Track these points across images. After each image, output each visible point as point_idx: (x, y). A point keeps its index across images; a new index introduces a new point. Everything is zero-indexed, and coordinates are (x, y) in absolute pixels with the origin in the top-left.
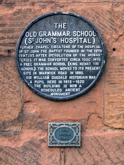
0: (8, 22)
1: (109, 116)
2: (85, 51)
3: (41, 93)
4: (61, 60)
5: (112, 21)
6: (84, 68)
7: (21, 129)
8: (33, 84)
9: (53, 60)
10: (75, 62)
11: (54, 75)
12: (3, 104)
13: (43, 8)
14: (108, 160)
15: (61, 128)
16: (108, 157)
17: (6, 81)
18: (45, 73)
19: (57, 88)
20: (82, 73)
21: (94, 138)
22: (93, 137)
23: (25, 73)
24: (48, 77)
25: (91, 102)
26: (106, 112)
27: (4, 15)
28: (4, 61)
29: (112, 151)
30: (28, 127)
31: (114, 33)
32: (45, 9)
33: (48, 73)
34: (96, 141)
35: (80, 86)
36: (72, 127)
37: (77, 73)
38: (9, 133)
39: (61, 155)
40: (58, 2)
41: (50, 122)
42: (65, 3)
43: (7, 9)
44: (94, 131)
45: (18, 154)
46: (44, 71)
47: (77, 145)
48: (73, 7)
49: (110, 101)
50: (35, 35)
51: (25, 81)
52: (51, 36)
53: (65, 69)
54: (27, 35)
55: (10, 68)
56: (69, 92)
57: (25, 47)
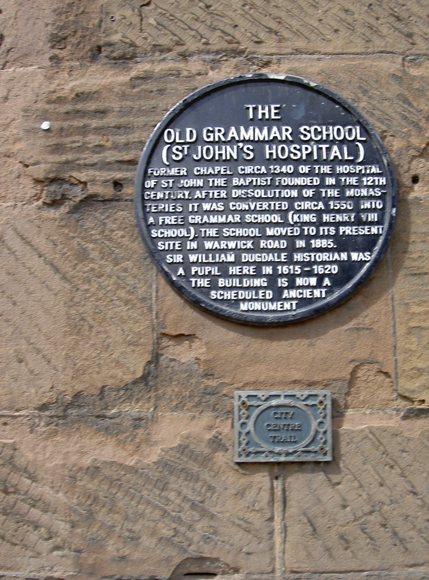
0: (116, 106)
1: (412, 369)
2: (338, 181)
3: (212, 303)
4: (269, 206)
5: (406, 101)
6: (337, 230)
7: (152, 409)
8: (187, 276)
10: (308, 211)
11: (247, 250)
12: (99, 336)
13: (212, 69)
14: (410, 498)
15: (271, 407)
16: (410, 489)
17: (108, 270)
18: (223, 246)
19: (257, 288)
20: (330, 245)
21: (371, 436)
22: (367, 431)
23: (164, 244)
24: (231, 255)
25: (357, 329)
26: (403, 356)
27: (105, 87)
28: (102, 214)
29: (422, 472)
30: (174, 403)
31: (413, 133)
32: (217, 70)
33: (232, 245)
34: (377, 443)
35: (327, 282)
36: (305, 403)
37: (282, 269)
38: (117, 420)
39: (272, 488)
40: (254, 53)
41: (238, 389)
42: (272, 55)
43: (113, 72)
44: (368, 412)
45: (145, 484)
46: (219, 238)
47: (321, 458)
48: (296, 65)
49: (412, 324)
50: (191, 137)
51: (163, 269)
52: (237, 139)
53: (281, 233)
54: (169, 138)
55: (121, 233)
56: (292, 299)
57: (162, 171)
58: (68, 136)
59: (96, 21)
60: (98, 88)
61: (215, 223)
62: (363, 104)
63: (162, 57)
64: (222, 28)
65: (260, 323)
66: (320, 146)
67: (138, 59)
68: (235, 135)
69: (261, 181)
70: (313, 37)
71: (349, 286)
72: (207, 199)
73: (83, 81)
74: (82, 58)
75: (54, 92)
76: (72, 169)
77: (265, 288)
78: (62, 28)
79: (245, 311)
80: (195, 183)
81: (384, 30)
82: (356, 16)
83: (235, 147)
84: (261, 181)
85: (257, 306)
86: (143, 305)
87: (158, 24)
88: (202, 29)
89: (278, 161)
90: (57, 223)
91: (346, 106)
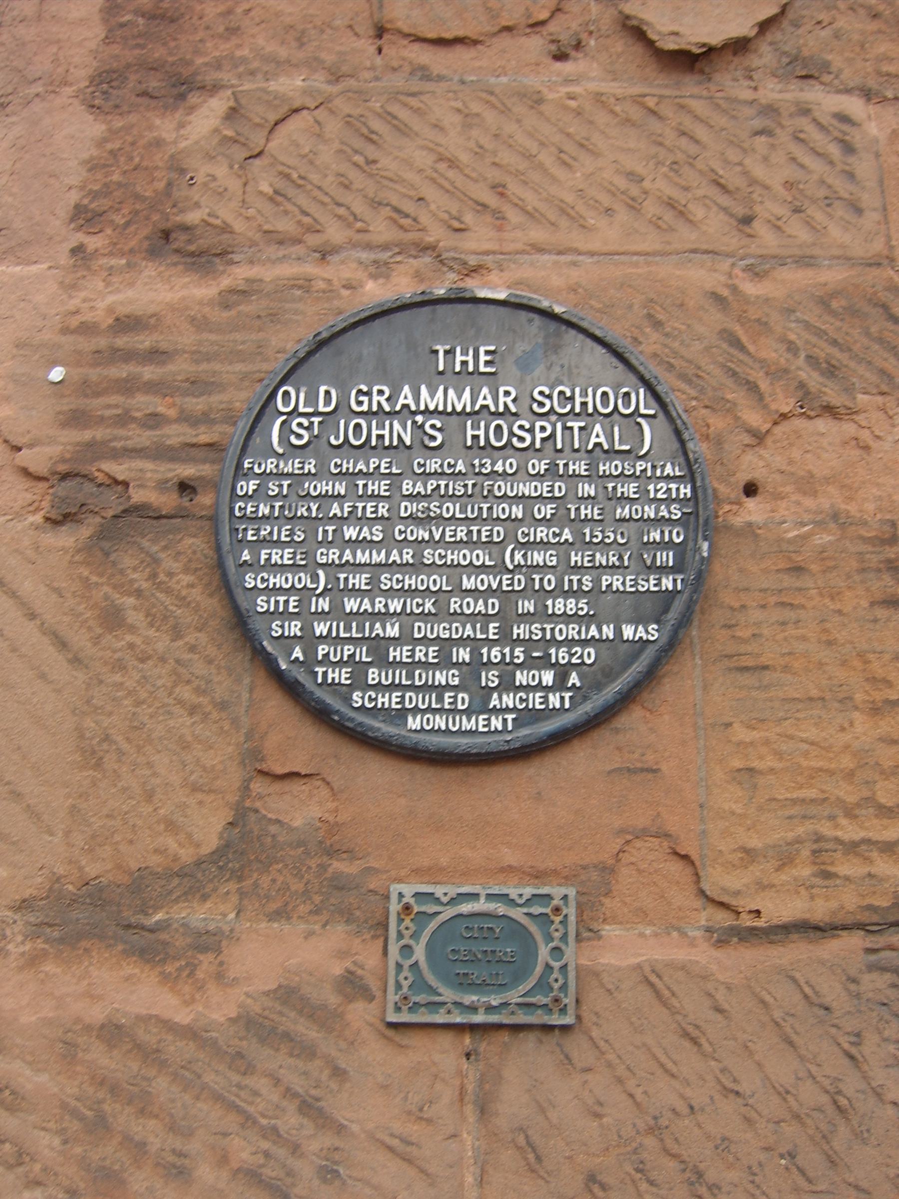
5: (737, 344)
6: (597, 581)
10: (544, 545)
11: (424, 616)
13: (374, 277)
15: (461, 915)
18: (379, 607)
19: (440, 690)
20: (582, 609)
23: (268, 602)
33: (395, 605)
36: (525, 910)
37: (554, 606)
38: (164, 936)
41: (400, 881)
42: (487, 253)
47: (556, 1020)
50: (327, 402)
53: (489, 585)
56: (507, 710)
57: (270, 465)
58: (97, 395)
59: (161, 185)
61: (365, 565)
62: (648, 347)
63: (280, 254)
66: (569, 424)
67: (236, 257)
68: (410, 401)
70: (564, 222)
72: (353, 516)
73: (130, 293)
74: (131, 251)
75: (77, 312)
76: (102, 457)
78: (95, 195)
79: (415, 731)
80: (330, 488)
81: (698, 212)
82: (646, 184)
83: (409, 423)
85: (440, 722)
86: (224, 715)
87: (276, 192)
88: (359, 207)
90: (68, 557)
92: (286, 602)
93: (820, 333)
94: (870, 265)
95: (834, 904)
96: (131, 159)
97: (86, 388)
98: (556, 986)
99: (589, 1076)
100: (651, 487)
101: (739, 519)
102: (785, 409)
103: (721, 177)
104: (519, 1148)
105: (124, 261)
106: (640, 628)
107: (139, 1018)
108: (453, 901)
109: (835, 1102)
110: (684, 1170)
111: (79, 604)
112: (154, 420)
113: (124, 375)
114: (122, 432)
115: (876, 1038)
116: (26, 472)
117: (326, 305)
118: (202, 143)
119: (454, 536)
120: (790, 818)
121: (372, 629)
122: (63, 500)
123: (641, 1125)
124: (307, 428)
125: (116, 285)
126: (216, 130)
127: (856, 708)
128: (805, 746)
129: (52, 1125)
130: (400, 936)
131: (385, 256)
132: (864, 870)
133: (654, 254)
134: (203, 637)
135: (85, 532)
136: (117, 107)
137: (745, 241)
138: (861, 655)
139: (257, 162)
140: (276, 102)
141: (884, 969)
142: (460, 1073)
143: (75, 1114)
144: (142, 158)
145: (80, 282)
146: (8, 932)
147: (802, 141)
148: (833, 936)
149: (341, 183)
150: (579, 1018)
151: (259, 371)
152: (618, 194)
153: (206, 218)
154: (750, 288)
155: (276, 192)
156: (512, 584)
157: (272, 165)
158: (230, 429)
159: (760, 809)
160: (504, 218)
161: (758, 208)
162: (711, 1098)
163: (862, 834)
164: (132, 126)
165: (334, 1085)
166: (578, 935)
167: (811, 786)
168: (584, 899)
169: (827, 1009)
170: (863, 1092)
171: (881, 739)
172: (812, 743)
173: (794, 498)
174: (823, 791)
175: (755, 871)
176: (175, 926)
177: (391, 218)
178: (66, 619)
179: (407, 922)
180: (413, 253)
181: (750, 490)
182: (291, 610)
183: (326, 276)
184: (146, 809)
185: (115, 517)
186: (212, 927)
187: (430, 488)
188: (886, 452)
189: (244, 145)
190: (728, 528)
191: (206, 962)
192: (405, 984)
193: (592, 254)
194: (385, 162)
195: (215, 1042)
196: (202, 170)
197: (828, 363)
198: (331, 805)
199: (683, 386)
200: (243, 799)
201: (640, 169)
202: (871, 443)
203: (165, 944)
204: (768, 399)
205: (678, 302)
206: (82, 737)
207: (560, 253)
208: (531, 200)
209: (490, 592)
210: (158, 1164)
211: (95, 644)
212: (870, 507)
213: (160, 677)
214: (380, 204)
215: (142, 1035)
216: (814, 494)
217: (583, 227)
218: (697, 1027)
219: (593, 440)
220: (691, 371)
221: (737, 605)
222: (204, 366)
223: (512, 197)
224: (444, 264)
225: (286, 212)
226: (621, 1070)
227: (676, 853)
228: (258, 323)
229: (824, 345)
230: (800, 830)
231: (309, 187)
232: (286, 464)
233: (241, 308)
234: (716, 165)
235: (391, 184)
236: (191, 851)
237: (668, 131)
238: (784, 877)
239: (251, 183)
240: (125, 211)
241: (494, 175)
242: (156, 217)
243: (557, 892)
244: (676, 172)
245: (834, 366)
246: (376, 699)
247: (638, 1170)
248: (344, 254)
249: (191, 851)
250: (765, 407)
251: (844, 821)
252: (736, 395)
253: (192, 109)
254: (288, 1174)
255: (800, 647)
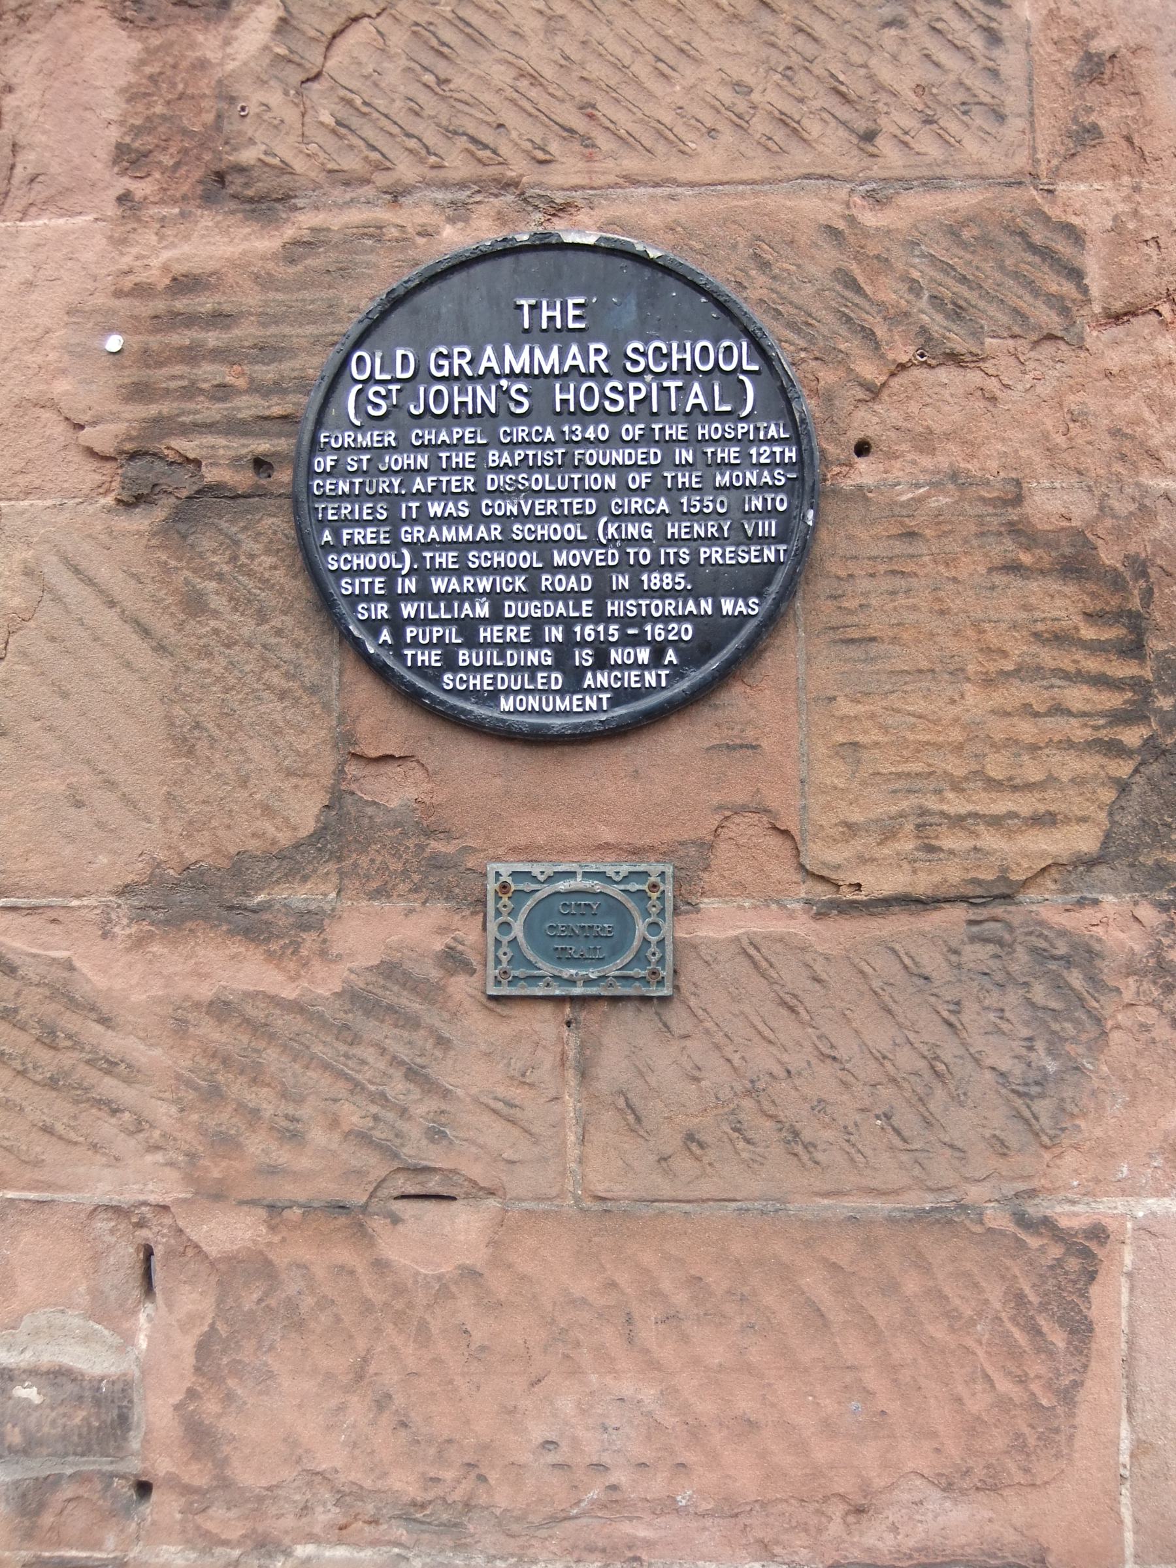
5: (853, 284)
6: (695, 554)
9: (509, 507)
10: (638, 517)
11: (515, 595)
13: (451, 220)
15: (558, 893)
18: (467, 585)
19: (533, 670)
22: (745, 942)
23: (352, 584)
27: (233, 263)
33: (484, 584)
36: (622, 887)
38: (266, 916)
41: (497, 859)
42: (575, 188)
46: (462, 570)
47: (654, 991)
50: (405, 367)
53: (582, 561)
56: (602, 689)
57: (347, 439)
58: (160, 364)
59: (209, 118)
60: (218, 266)
61: (452, 542)
62: (754, 294)
63: (348, 197)
64: (471, 131)
65: (537, 735)
66: (666, 384)
67: (300, 202)
68: (494, 364)
69: (546, 457)
70: (661, 148)
71: (714, 664)
72: (437, 492)
73: (186, 248)
74: (184, 198)
75: (130, 272)
76: (171, 433)
77: (547, 668)
78: (137, 131)
79: (509, 712)
80: (412, 462)
81: (814, 128)
82: (755, 97)
83: (493, 388)
84: (546, 457)
85: (533, 702)
86: (314, 700)
87: (338, 123)
88: (432, 138)
89: (581, 415)
90: (144, 541)
91: (722, 299)
92: (371, 584)
93: (947, 269)
94: (1009, 185)
95: (937, 878)
96: (174, 85)
97: (147, 357)
98: (653, 959)
99: (688, 1043)
100: (753, 451)
101: (850, 482)
102: (904, 359)
103: (842, 83)
104: (619, 1110)
105: (176, 210)
106: (740, 602)
107: (247, 995)
108: (550, 879)
109: (932, 1067)
110: (781, 1130)
111: (159, 589)
112: (223, 391)
113: (187, 342)
114: (190, 406)
115: (976, 1007)
116: (91, 452)
117: (400, 256)
118: (252, 64)
119: (544, 509)
120: (894, 792)
121: (460, 609)
122: (133, 481)
123: (739, 1088)
124: (384, 398)
125: (171, 239)
126: (266, 48)
127: (968, 680)
128: (913, 720)
129: (167, 1095)
130: (498, 913)
131: (463, 195)
132: (968, 844)
133: (762, 182)
134: (289, 620)
135: (160, 513)
136: (152, 19)
137: (867, 162)
138: (976, 625)
139: (315, 86)
140: (332, 9)
141: (986, 940)
142: (560, 1039)
143: (189, 1084)
144: (186, 85)
145: (131, 235)
146: (113, 916)
147: (939, 31)
148: (935, 909)
149: (411, 109)
150: (677, 988)
151: (332, 334)
152: (723, 109)
153: (263, 157)
154: (870, 219)
155: (338, 123)
156: (606, 560)
157: (332, 88)
158: (304, 400)
159: (864, 783)
160: (594, 146)
161: (883, 121)
162: (809, 1063)
163: (970, 808)
164: (171, 44)
165: (438, 1053)
166: (675, 908)
167: (917, 760)
168: (683, 874)
169: (926, 978)
170: (961, 1057)
171: (993, 712)
172: (920, 717)
173: (909, 457)
174: (929, 765)
175: (857, 845)
176: (277, 906)
177: (467, 150)
178: (148, 606)
179: (505, 900)
180: (495, 191)
181: (862, 449)
182: (377, 592)
183: (399, 222)
184: (242, 794)
185: (189, 498)
186: (313, 907)
187: (517, 458)
188: (1014, 402)
189: (299, 65)
190: (836, 492)
191: (309, 939)
192: (504, 959)
193: (692, 185)
194: (459, 81)
195: (321, 1016)
196: (254, 98)
197: (955, 304)
198: (426, 786)
199: (791, 336)
200: (338, 782)
201: (749, 79)
202: (998, 393)
203: (267, 923)
204: (884, 347)
205: (788, 239)
206: (172, 724)
207: (657, 185)
208: (624, 121)
209: (583, 567)
210: (272, 1128)
211: (179, 631)
212: (993, 465)
213: (247, 662)
214: (455, 133)
215: (249, 1010)
216: (932, 452)
217: (683, 152)
218: (795, 996)
219: (692, 401)
220: (801, 318)
221: (843, 574)
222: (273, 330)
223: (604, 120)
224: (528, 203)
225: (351, 147)
226: (719, 1037)
227: (775, 828)
228: (328, 278)
229: (950, 282)
230: (904, 804)
231: (375, 115)
232: (364, 437)
233: (309, 262)
234: (836, 68)
235: (466, 109)
236: (289, 834)
237: (782, 27)
238: (886, 851)
239: (311, 112)
240: (173, 150)
241: (582, 92)
242: (207, 157)
243: (654, 868)
244: (789, 79)
245: (960, 307)
246: (467, 681)
247: (735, 1130)
248: (418, 195)
249: (289, 834)
250: (882, 357)
251: (950, 795)
252: (848, 344)
253: (237, 20)
254: (397, 1136)
255: (910, 617)
